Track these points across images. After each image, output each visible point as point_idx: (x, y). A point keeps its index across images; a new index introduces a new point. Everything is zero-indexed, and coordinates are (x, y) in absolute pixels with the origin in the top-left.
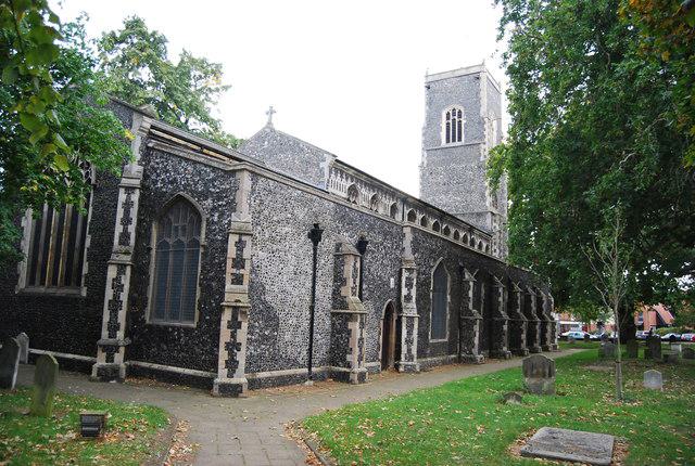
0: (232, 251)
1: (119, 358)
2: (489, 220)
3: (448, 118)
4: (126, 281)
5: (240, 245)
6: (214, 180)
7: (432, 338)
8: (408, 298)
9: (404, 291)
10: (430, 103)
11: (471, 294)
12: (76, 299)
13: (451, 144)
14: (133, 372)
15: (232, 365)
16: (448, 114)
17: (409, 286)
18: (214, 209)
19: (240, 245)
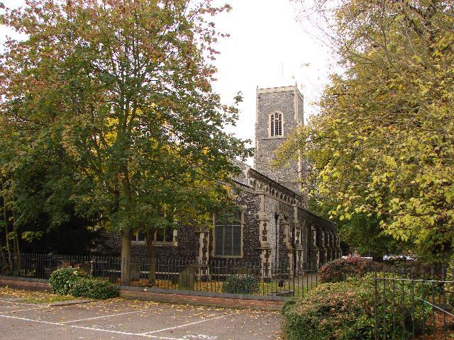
0: (261, 228)
1: (207, 272)
2: (300, 187)
3: (272, 119)
4: (208, 239)
5: (265, 225)
6: (247, 197)
7: (139, 240)
8: (298, 241)
9: (296, 238)
10: (260, 107)
11: (315, 238)
12: (171, 248)
13: (275, 137)
14: (213, 278)
15: (267, 271)
16: (272, 116)
17: (298, 236)
18: (248, 210)
19: (265, 225)
